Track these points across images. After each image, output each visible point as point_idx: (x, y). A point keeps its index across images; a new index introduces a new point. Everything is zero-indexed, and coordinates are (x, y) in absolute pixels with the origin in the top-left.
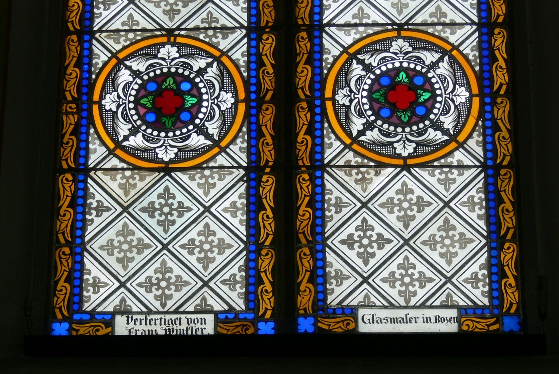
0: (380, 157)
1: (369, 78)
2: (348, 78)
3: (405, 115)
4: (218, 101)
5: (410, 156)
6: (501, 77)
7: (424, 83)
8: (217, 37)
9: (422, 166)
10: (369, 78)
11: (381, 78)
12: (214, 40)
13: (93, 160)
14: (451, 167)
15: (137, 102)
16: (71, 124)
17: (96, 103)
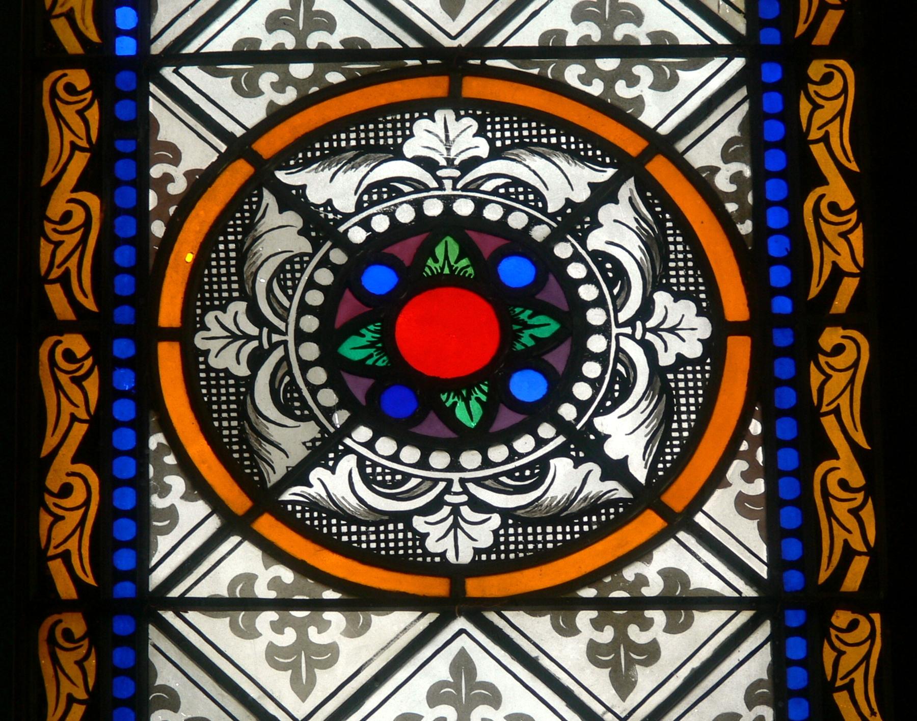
0: (367, 567)
1: (325, 262)
2: (248, 270)
3: (467, 400)
4: (645, 330)
5: (482, 566)
6: (841, 251)
7: (539, 283)
8: (633, 81)
9: (534, 602)
10: (325, 262)
11: (380, 263)
12: (622, 89)
13: (168, 553)
14: (637, 605)
15: (575, 328)
16: (74, 418)
17: (738, 328)
